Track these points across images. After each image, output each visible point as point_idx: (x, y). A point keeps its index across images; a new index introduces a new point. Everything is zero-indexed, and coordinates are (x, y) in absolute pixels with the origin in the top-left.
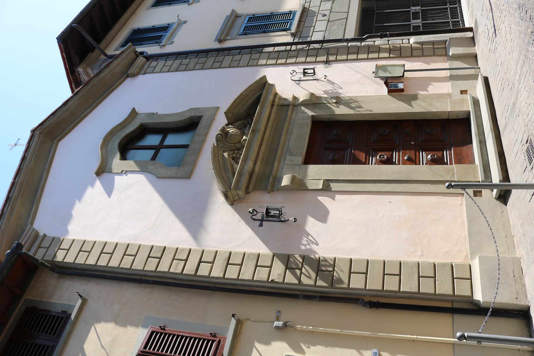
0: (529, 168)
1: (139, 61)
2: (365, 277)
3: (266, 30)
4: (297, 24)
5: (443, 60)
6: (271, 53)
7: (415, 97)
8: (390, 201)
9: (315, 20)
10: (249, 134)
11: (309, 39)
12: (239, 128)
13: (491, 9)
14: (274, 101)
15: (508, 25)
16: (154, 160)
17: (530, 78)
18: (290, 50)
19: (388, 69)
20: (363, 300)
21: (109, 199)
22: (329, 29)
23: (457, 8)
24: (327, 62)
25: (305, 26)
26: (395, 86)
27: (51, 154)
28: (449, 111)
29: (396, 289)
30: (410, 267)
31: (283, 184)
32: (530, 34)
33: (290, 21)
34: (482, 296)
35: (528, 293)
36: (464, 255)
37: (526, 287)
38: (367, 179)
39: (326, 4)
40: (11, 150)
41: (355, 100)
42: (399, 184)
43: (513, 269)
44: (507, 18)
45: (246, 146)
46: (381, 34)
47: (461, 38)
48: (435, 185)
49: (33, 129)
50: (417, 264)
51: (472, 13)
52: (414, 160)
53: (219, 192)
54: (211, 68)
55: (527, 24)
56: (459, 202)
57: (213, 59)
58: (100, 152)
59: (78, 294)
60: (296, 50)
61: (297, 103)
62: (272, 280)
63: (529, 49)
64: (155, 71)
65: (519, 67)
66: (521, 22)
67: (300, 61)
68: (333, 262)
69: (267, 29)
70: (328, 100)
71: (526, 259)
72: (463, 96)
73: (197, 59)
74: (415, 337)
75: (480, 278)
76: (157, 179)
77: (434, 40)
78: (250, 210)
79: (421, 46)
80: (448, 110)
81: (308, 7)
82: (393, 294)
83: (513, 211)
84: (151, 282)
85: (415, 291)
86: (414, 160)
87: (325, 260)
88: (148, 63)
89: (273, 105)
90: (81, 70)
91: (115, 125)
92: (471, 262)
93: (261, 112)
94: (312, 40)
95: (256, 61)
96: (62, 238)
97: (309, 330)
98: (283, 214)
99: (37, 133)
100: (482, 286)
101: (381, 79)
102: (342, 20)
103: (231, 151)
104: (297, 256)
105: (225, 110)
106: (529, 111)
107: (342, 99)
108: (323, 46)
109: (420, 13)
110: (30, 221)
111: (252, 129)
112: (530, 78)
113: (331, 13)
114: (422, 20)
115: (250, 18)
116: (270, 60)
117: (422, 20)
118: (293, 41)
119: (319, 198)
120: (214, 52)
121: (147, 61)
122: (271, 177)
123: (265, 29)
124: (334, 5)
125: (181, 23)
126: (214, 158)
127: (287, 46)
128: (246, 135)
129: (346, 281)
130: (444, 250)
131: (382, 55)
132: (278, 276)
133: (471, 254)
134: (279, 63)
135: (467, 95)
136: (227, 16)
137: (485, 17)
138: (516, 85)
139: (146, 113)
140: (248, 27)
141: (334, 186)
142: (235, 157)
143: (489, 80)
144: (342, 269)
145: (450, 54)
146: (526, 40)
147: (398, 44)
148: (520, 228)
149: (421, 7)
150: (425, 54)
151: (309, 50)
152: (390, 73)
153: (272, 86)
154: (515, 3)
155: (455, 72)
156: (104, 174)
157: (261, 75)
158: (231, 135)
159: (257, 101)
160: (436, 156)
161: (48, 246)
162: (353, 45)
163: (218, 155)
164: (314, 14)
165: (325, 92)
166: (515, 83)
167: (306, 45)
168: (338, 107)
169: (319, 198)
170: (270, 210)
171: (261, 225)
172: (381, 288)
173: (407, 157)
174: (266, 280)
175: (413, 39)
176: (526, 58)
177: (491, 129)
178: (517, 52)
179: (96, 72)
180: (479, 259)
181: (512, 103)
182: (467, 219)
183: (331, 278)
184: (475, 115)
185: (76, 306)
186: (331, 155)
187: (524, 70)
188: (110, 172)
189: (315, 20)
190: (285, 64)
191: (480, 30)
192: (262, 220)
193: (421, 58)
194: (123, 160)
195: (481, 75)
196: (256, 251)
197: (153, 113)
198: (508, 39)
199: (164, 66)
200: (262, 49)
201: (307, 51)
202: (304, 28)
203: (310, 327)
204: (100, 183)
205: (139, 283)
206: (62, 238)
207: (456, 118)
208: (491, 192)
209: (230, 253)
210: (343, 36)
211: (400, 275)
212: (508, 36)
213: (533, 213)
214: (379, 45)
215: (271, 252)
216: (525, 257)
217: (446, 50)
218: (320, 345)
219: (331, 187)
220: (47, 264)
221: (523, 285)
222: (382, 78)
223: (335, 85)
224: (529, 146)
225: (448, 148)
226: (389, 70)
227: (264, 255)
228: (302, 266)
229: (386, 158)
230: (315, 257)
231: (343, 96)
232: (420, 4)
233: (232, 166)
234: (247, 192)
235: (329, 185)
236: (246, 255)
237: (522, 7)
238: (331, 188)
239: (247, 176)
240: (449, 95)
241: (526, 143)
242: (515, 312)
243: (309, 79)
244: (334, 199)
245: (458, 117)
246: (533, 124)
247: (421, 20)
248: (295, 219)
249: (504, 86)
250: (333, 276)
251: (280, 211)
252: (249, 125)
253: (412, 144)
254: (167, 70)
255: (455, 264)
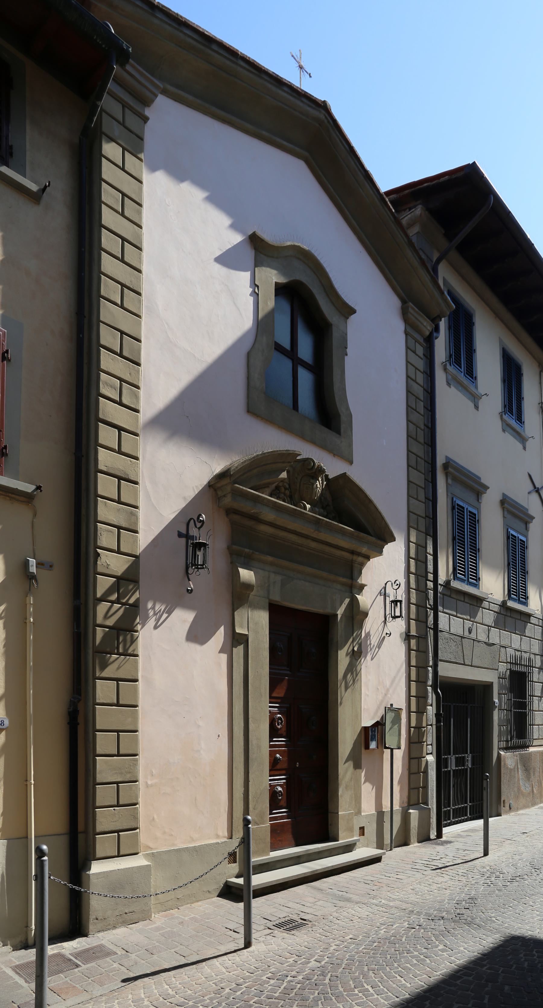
0: (270, 924)
1: (425, 324)
2: (113, 703)
3: (457, 540)
4: (462, 589)
5: (403, 801)
6: (425, 549)
7: (358, 766)
8: (220, 735)
9: (465, 617)
10: (314, 515)
11: (440, 608)
12: (323, 498)
13: (466, 861)
14: (359, 554)
15: (449, 885)
16: (275, 349)
17: (385, 918)
18: (427, 580)
19: (396, 726)
20: (79, 700)
21: (213, 260)
22: (452, 639)
23: (466, 815)
24: (408, 637)
25: (458, 601)
26: (373, 737)
27: (285, 143)
28: (338, 813)
29: (99, 750)
30: (131, 769)
31: (241, 570)
32: (441, 915)
33: (466, 579)
34: (97, 873)
35: (105, 932)
36: (151, 845)
37: (113, 929)
38: (249, 701)
39: (484, 632)
40: (293, 56)
41: (356, 680)
42: (243, 747)
43: (136, 911)
44: (457, 883)
45: (296, 510)
46: (442, 714)
47: (429, 824)
48: (243, 799)
49: (328, 107)
50: (135, 779)
51: (459, 836)
52: (275, 768)
53: (228, 463)
54: (409, 451)
55: (453, 910)
56: (221, 834)
57: (421, 454)
58: (289, 243)
59: (47, 184)
60: (427, 589)
61: (355, 591)
62: (98, 555)
63: (422, 914)
64: (409, 351)
65: (398, 903)
66: (455, 902)
67: (411, 595)
68: (132, 653)
69: (458, 542)
70: (358, 639)
71: (150, 927)
72: (357, 831)
73: (422, 427)
74: (33, 782)
75: (121, 869)
76: (247, 352)
77: (429, 788)
78: (204, 516)
79: (422, 770)
80: (341, 812)
81: (482, 606)
82: (91, 745)
83: (211, 906)
84: (81, 336)
85: (97, 778)
86: (275, 768)
87: (134, 640)
88: (422, 341)
89: (353, 552)
90: (418, 213)
91: (331, 275)
92: (142, 854)
93: (343, 533)
94: (439, 613)
95: (415, 526)
96: (142, 156)
97: (28, 618)
98: (198, 571)
99: (321, 115)
100: (111, 871)
101: (383, 716)
102: (462, 657)
103: (289, 485)
104: (137, 595)
105: (349, 473)
106: (343, 920)
107: (357, 660)
108: (429, 630)
109: (463, 768)
110: (169, 87)
111: (320, 519)
112: (386, 918)
113: (473, 641)
114: (454, 770)
115: (475, 515)
116: (414, 547)
117: (454, 771)
118: (440, 584)
119: (222, 629)
120: (431, 456)
121: (425, 337)
122: (251, 551)
123: (458, 539)
124: (482, 645)
125: (475, 399)
126: (279, 454)
127: (432, 575)
128: (312, 510)
129: (104, 675)
130: (156, 817)
131: (413, 716)
132: (105, 564)
133: (153, 853)
134: (411, 562)
135: (358, 835)
136: (480, 478)
137: (456, 854)
138: (374, 901)
139: (346, 334)
140: (462, 513)
141: (239, 651)
142: (279, 491)
143: (377, 864)
144: (122, 667)
145: (411, 811)
146: (433, 910)
147: (426, 739)
148: (190, 917)
149: (470, 769)
150: (412, 776)
151: (425, 609)
152: (390, 729)
153: (380, 553)
154: (476, 893)
155: (387, 819)
156: (253, 252)
157: (396, 535)
158: (313, 484)
159: (359, 527)
160: (280, 798)
161: (128, 124)
162: (429, 675)
163: (283, 462)
164: (473, 615)
165: (368, 635)
166: (377, 900)
167: (432, 604)
168: (347, 655)
169: (222, 629)
170: (204, 550)
171: (180, 535)
172: (98, 727)
173: (280, 758)
174: (99, 544)
175: (431, 759)
176: (410, 911)
177: (317, 870)
178: (416, 900)
179: (414, 240)
180: (147, 865)
181: (351, 896)
182: (199, 846)
183: (108, 650)
184: (333, 849)
185: (24, 178)
186: (282, 646)
187: (394, 911)
188: (258, 263)
189: (465, 617)
190: (408, 572)
191: (440, 848)
192: (187, 536)
193: (408, 771)
194: (276, 290)
195: (384, 853)
196: (141, 527)
197: (346, 348)
198: (431, 887)
199: (416, 368)
200: (432, 534)
201: (425, 606)
202: (455, 600)
203: (33, 619)
204: (239, 241)
205: (76, 313)
206: (142, 156)
207: (330, 823)
208: (235, 876)
209: (136, 483)
210: (442, 659)
211: (119, 755)
212: (435, 886)
213: (212, 933)
214: (426, 713)
215: (140, 551)
216: (153, 926)
217: (416, 805)
218: (6, 635)
219: (238, 647)
220: (95, 120)
221: (115, 925)
222: (383, 718)
223: (377, 649)
224: (298, 923)
225: (290, 813)
226: (394, 727)
227: (136, 541)
228: (123, 604)
229: (278, 728)
230: (137, 624)
231: (362, 660)
232: (474, 766)
233: (267, 486)
234: (229, 512)
235: (240, 644)
236: (134, 510)
237: (473, 902)
238: (236, 647)
239: (252, 512)
240: (359, 812)
241: (301, 919)
242: (78, 917)
243: (387, 610)
244: (221, 651)
245: (331, 825)
246: (326, 926)
247: (455, 768)
248: (192, 590)
249: (371, 884)
250: (111, 654)
251: (203, 566)
252: (325, 513)
253: (296, 764)
254: (410, 375)
255: (138, 832)
